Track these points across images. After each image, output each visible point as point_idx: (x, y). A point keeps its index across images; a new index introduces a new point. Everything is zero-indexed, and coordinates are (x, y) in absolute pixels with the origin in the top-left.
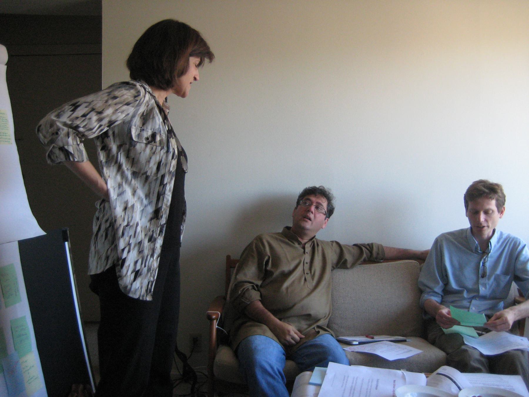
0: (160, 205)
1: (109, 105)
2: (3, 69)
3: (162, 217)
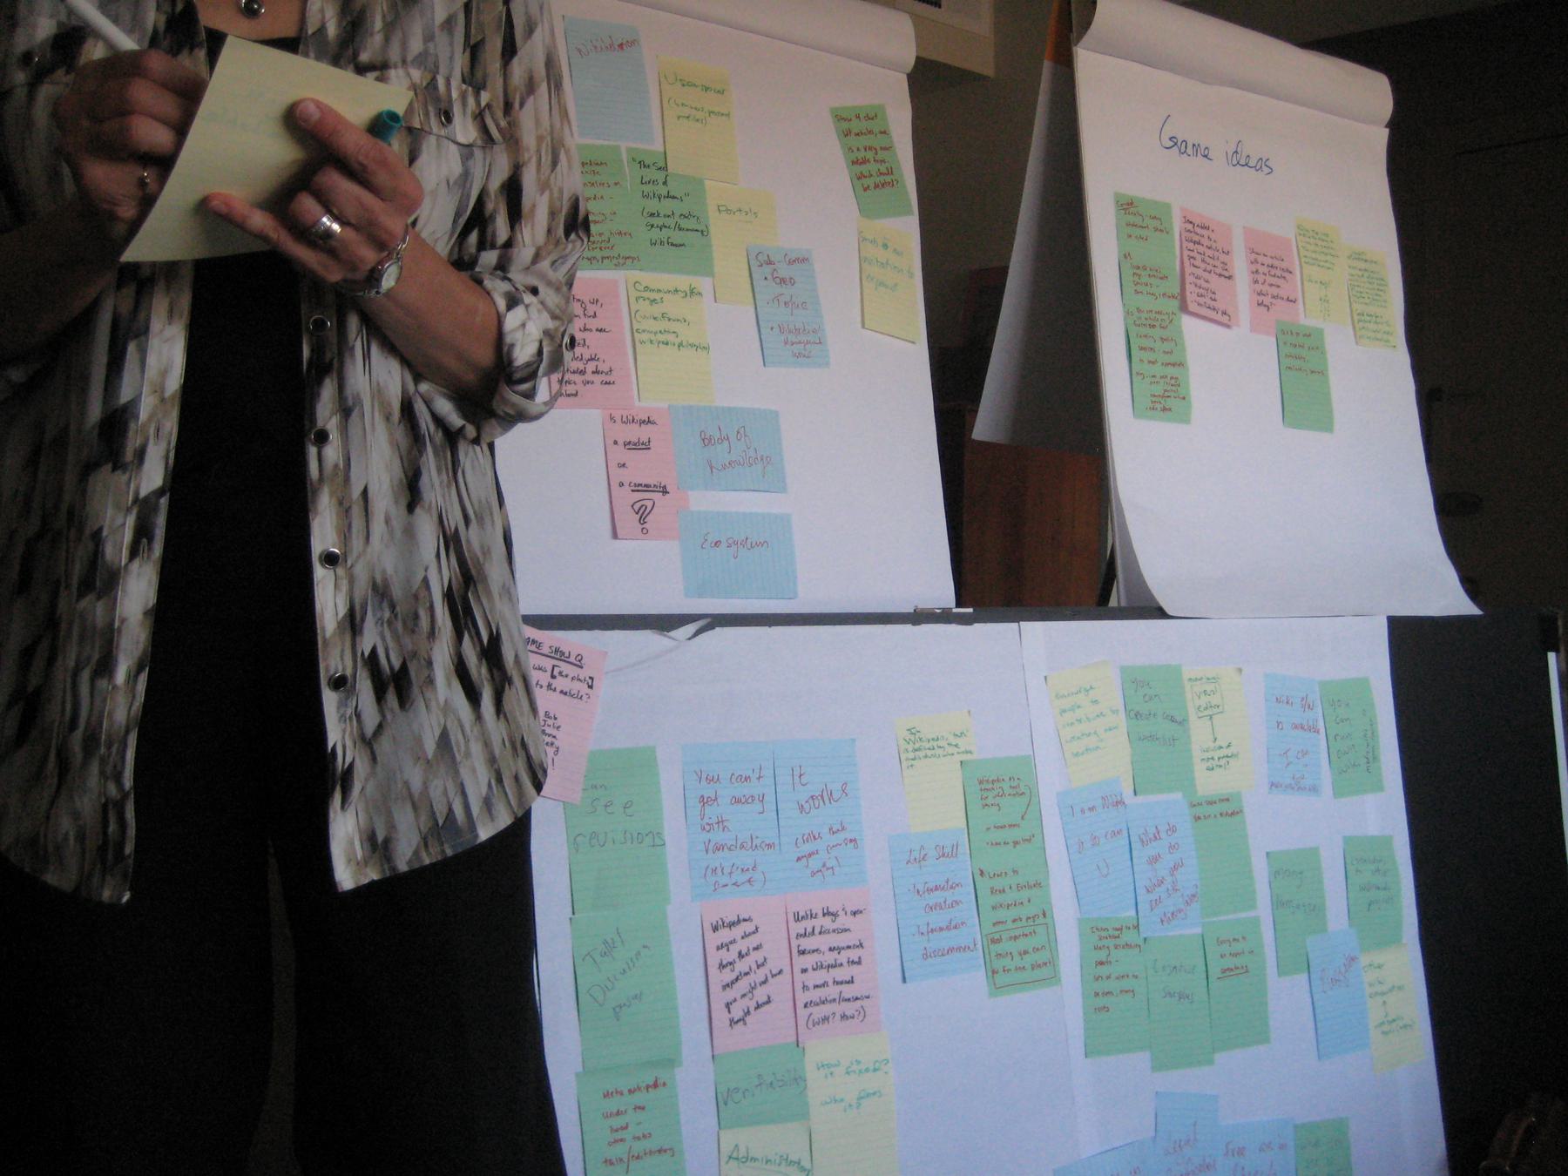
0: (125, 395)
2: (1380, 137)
3: (141, 454)
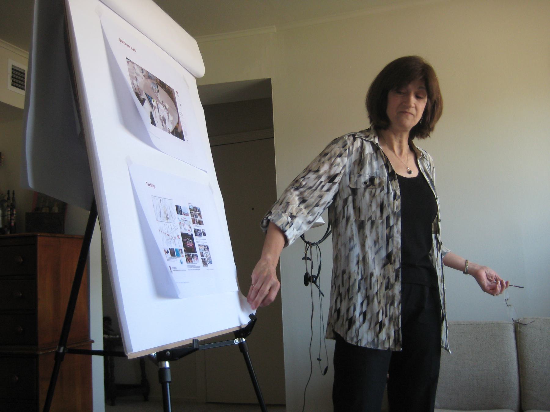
1: (323, 162)
3: (395, 261)
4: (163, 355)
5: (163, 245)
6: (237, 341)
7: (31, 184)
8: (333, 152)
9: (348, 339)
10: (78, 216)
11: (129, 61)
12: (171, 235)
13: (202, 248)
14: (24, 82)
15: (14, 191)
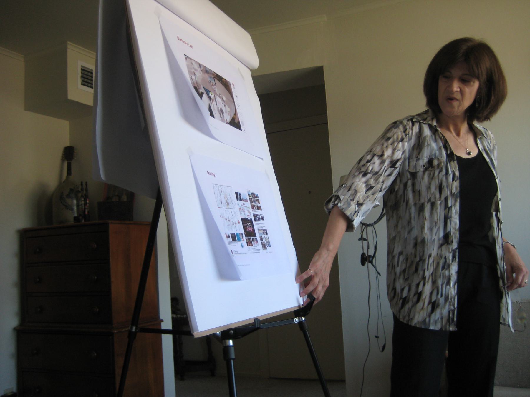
0: (448, 229)
3: (452, 242)
4: (226, 334)
5: (225, 230)
6: (296, 320)
7: (103, 177)
8: (395, 137)
9: (401, 317)
10: (145, 204)
11: (187, 57)
12: (231, 220)
13: (262, 232)
14: (92, 80)
15: (86, 183)
